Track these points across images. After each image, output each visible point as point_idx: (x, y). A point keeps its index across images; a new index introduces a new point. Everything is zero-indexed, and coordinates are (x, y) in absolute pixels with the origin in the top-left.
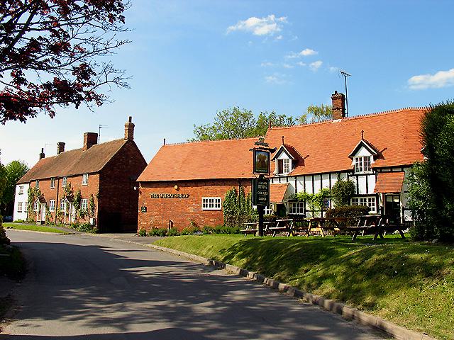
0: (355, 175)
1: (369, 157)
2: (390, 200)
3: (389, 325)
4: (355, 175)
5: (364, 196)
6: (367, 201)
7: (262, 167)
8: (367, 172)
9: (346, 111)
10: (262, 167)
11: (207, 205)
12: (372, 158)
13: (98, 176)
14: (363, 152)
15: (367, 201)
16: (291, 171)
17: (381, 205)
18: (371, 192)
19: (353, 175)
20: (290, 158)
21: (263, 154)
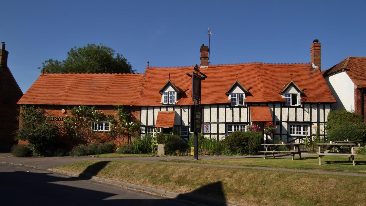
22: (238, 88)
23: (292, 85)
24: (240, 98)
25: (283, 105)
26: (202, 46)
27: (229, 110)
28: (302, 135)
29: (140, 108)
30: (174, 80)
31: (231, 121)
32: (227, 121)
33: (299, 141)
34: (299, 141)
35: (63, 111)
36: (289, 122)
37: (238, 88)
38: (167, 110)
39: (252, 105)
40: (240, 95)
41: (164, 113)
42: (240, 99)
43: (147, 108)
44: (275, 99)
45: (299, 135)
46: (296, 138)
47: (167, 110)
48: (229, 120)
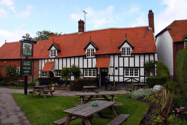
0: (87, 58)
1: (94, 50)
2: (103, 71)
3: (3, 109)
4: (87, 58)
5: (90, 68)
6: (92, 71)
7: (28, 52)
8: (93, 57)
9: (85, 29)
10: (28, 52)
11: (44, 75)
12: (95, 50)
13: (144, 68)
14: (91, 47)
15: (92, 71)
16: (56, 55)
17: (99, 73)
18: (94, 66)
19: (86, 58)
20: (56, 49)
21: (28, 44)
22: (90, 45)
23: (126, 41)
24: (54, 53)
25: (120, 56)
26: (79, 20)
27: (116, 58)
28: (134, 76)
29: (38, 60)
30: (93, 40)
31: (86, 67)
32: (84, 67)
33: (132, 80)
34: (132, 80)
35: (5, 62)
36: (83, 69)
37: (90, 45)
38: (48, 61)
39: (105, 56)
40: (93, 50)
41: (49, 63)
42: (54, 53)
43: (42, 59)
44: (114, 52)
45: (132, 76)
46: (135, 79)
47: (48, 61)
48: (126, 65)
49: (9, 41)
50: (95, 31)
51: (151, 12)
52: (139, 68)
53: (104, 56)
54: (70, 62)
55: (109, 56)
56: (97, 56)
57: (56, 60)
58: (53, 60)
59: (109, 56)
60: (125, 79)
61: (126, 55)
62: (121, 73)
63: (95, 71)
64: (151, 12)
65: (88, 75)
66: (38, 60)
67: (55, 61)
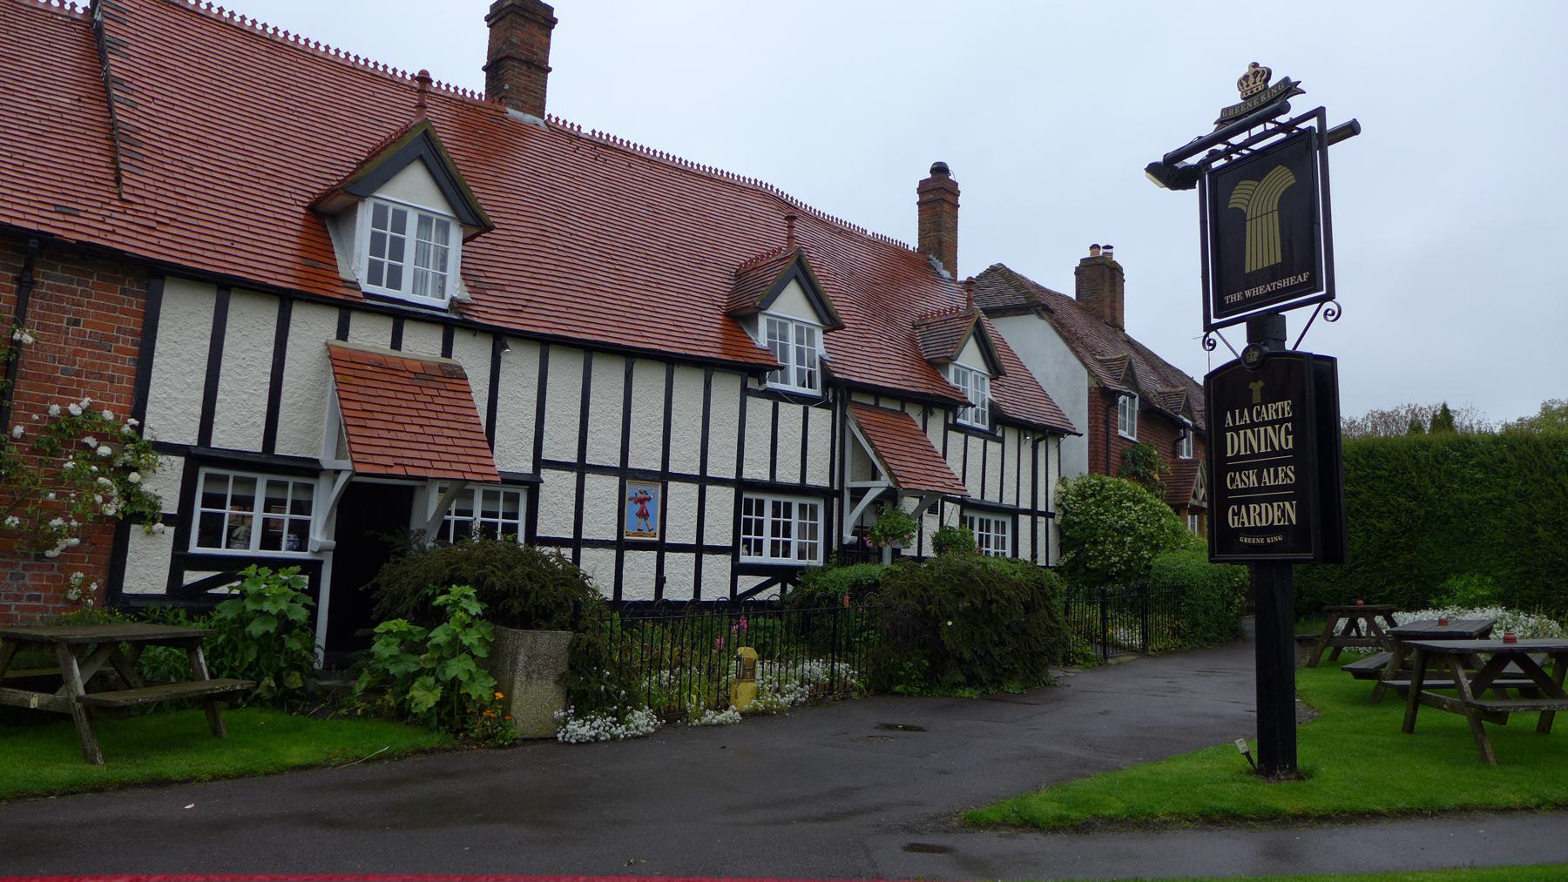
27: (726, 392)
34: (783, 589)
45: (780, 560)
49: (484, 62)
50: (606, 147)
51: (940, 170)
52: (664, 476)
53: (877, 403)
54: (269, 351)
55: (903, 407)
56: (838, 392)
57: (472, 356)
58: (422, 345)
59: (903, 407)
60: (746, 583)
61: (793, 387)
62: (720, 530)
63: (814, 516)
64: (940, 170)
65: (767, 548)
66: (150, 276)
67: (447, 351)
